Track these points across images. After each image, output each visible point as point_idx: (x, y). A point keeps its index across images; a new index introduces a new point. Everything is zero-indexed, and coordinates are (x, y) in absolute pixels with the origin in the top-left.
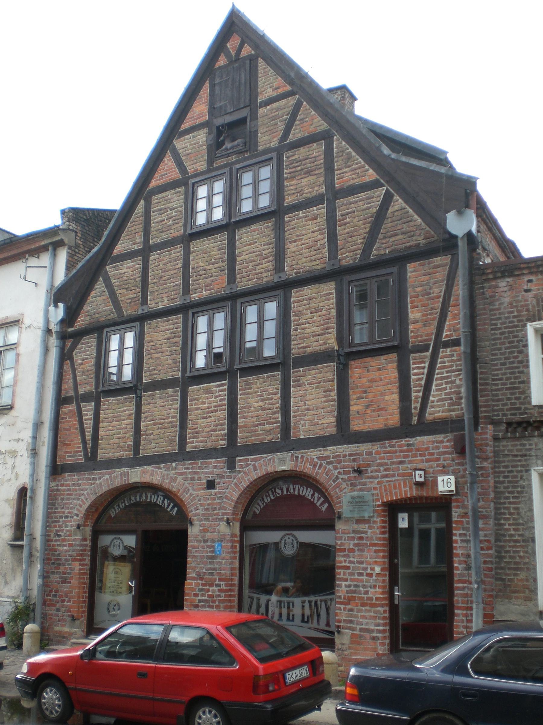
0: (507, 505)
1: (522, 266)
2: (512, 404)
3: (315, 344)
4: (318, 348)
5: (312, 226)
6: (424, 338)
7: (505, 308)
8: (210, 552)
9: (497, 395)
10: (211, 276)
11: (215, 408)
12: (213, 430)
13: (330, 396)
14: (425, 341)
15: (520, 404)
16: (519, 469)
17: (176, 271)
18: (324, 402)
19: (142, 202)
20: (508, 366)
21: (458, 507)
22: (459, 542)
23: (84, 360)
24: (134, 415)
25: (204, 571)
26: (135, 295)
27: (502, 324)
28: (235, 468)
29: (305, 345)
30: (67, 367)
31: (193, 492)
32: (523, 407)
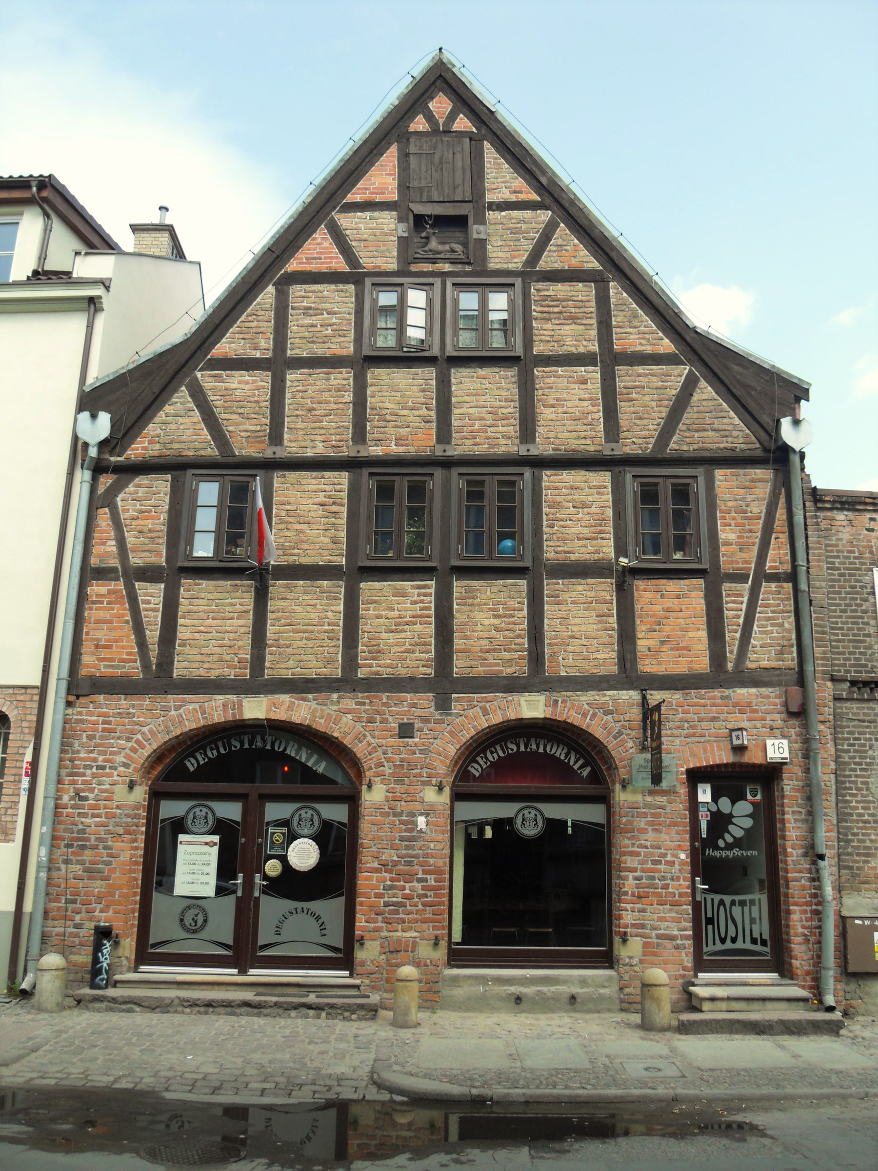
0: (853, 779)
1: (867, 500)
2: (856, 659)
3: (583, 550)
4: (588, 556)
5: (578, 391)
6: (741, 565)
7: (843, 546)
8: (406, 831)
9: (838, 647)
10: (408, 427)
11: (413, 619)
12: (408, 651)
13: (607, 622)
14: (742, 569)
15: (866, 660)
16: (868, 736)
17: (341, 406)
18: (598, 630)
19: (271, 289)
20: (849, 614)
21: (790, 779)
22: (793, 821)
23: (141, 512)
24: (251, 612)
25: (395, 858)
26: (259, 428)
27: (840, 563)
28: (450, 709)
29: (566, 549)
30: (104, 517)
31: (372, 741)
32: (870, 664)
